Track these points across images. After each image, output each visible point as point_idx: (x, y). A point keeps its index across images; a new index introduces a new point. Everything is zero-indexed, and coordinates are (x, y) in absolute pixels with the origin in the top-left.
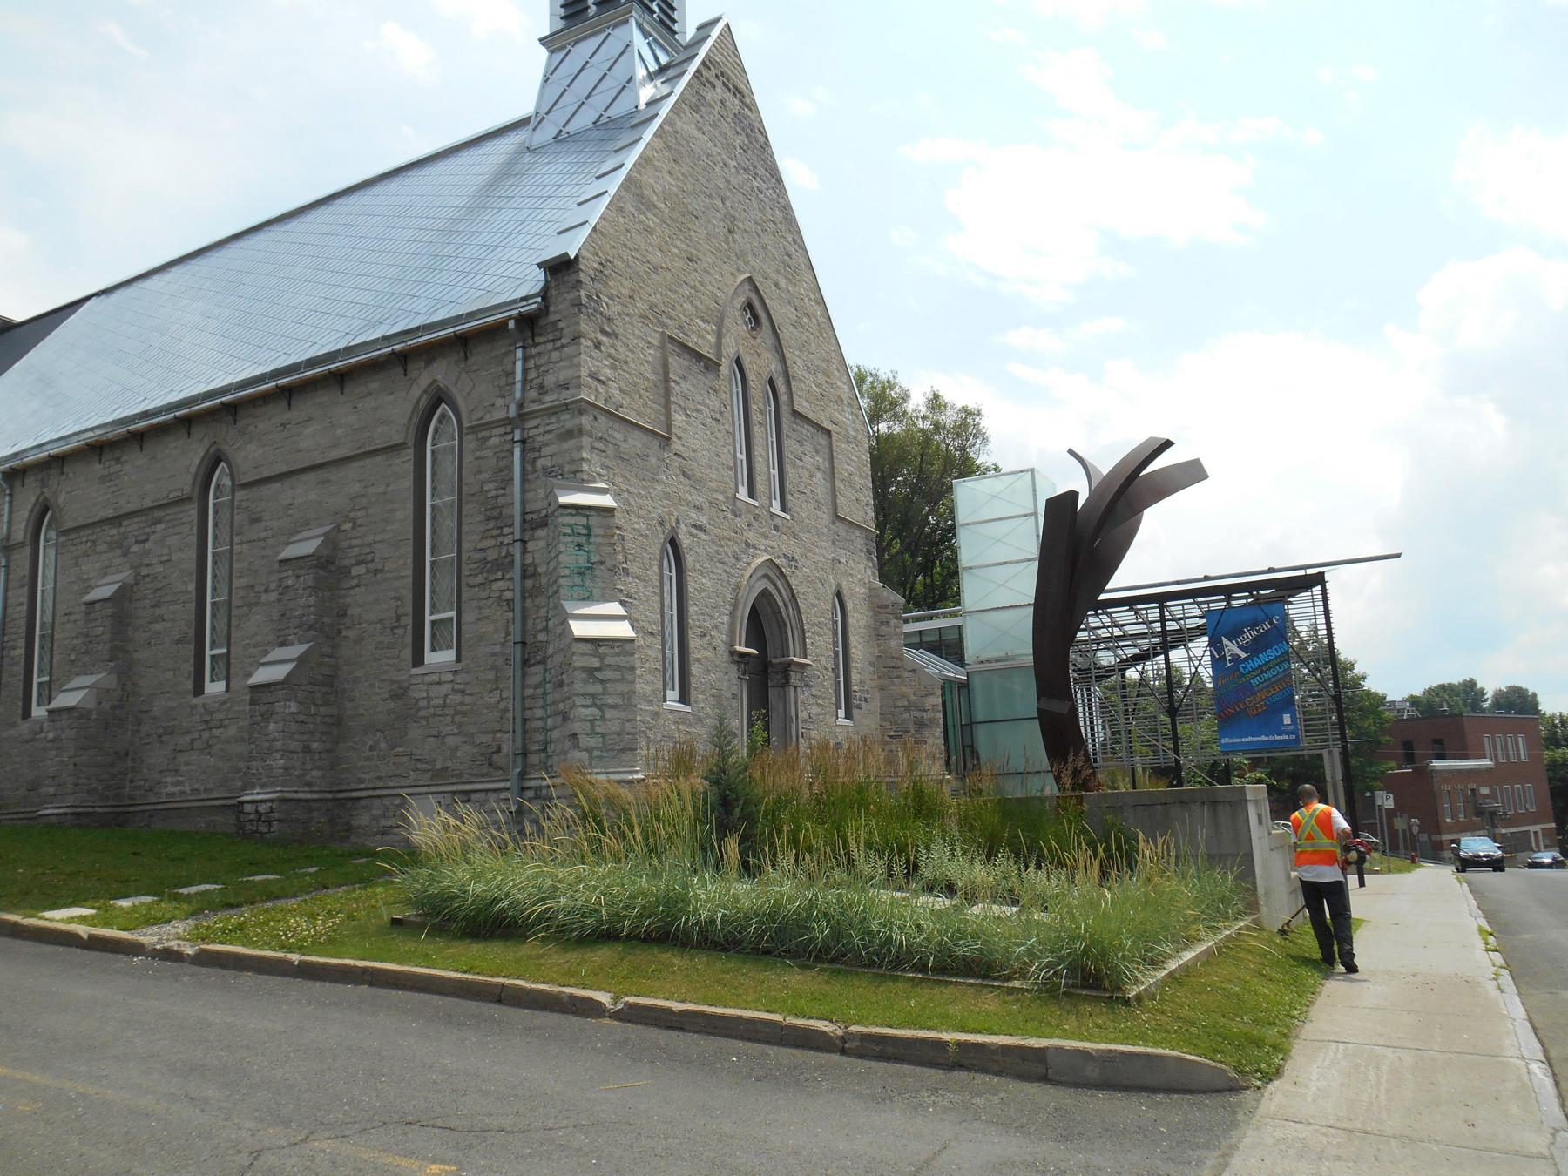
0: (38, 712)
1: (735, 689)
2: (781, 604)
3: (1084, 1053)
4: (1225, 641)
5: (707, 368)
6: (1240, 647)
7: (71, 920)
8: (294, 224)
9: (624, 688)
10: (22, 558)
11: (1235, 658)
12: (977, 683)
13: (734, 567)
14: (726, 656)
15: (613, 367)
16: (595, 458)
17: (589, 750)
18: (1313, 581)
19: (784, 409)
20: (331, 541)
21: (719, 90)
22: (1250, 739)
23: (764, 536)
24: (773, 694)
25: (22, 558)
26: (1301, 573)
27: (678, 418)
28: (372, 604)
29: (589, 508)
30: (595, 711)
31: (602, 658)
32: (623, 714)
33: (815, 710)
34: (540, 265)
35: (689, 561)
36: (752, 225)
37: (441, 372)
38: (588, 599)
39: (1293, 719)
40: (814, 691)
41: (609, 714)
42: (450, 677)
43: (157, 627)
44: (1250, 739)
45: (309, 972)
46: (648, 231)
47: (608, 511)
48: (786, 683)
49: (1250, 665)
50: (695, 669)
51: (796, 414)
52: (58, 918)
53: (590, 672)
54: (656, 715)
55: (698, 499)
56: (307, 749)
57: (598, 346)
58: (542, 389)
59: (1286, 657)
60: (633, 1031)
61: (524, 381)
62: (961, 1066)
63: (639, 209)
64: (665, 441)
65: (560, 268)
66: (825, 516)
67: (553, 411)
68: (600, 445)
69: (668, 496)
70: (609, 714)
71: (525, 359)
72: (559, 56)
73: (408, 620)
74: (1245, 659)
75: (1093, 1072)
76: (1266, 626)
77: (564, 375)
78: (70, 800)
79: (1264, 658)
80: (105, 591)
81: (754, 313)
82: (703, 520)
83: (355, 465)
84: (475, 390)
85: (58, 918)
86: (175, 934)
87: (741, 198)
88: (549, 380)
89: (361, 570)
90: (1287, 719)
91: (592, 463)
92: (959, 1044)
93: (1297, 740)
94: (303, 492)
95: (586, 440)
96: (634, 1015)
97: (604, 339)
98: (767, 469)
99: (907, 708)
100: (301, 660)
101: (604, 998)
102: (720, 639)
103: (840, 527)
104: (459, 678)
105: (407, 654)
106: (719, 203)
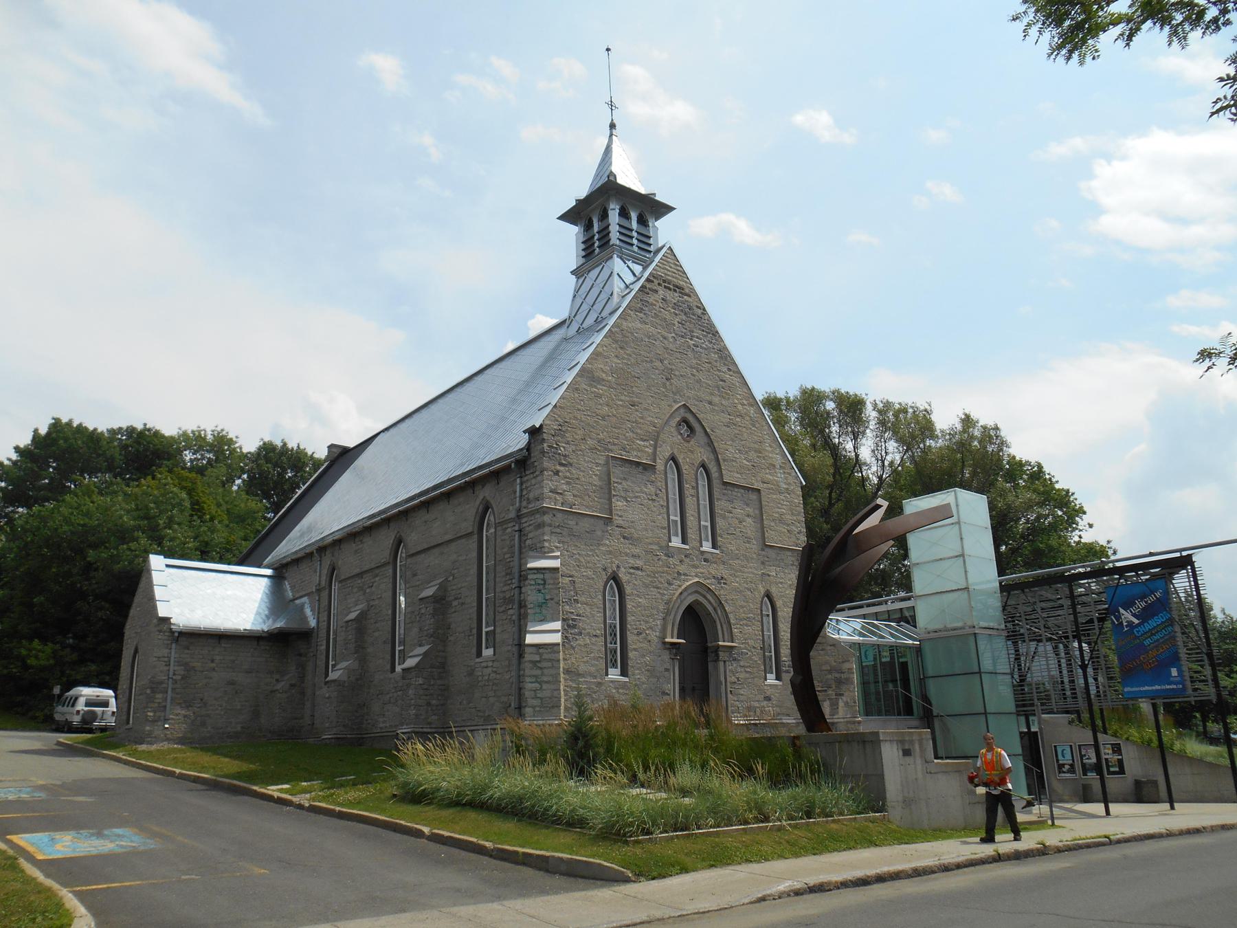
0: (398, 668)
1: (668, 666)
2: (710, 609)
3: (561, 859)
4: (1122, 611)
5: (645, 469)
6: (1134, 615)
7: (281, 791)
8: (433, 407)
9: (552, 672)
10: (325, 594)
11: (1130, 624)
12: (927, 648)
13: (667, 589)
14: (660, 645)
15: (568, 483)
16: (554, 538)
17: (534, 707)
18: (1184, 562)
19: (716, 483)
20: (443, 587)
21: (661, 292)
22: (1147, 688)
23: (695, 567)
24: (710, 665)
25: (325, 594)
26: (1178, 555)
27: (619, 504)
28: (461, 620)
29: (544, 569)
30: (537, 685)
31: (541, 655)
32: (553, 687)
33: (742, 676)
34: (525, 432)
35: (628, 589)
36: (688, 370)
37: (486, 492)
38: (544, 620)
39: (1180, 671)
41: (545, 686)
42: (490, 664)
43: (376, 634)
44: (1147, 688)
45: (341, 816)
46: (599, 396)
47: (555, 570)
48: (717, 660)
49: (1142, 629)
50: (631, 655)
51: (725, 484)
52: (273, 790)
53: (534, 663)
54: (599, 684)
55: (637, 551)
56: (429, 704)
57: (557, 473)
58: (529, 501)
59: (1171, 622)
60: (433, 846)
61: (521, 496)
62: (524, 864)
63: (591, 385)
64: (609, 521)
65: (534, 432)
66: (755, 546)
67: (532, 513)
68: (558, 530)
69: (610, 552)
70: (545, 686)
71: (521, 484)
72: (581, 280)
73: (475, 631)
74: (1139, 625)
75: (563, 868)
76: (1152, 599)
77: (537, 493)
78: (334, 731)
79: (1153, 623)
80: (353, 616)
81: (689, 425)
82: (639, 563)
83: (454, 544)
84: (503, 501)
85: (273, 790)
86: (304, 799)
87: (679, 355)
88: (531, 496)
89: (455, 603)
90: (1174, 672)
91: (550, 541)
92: (524, 854)
93: (1184, 689)
94: (432, 559)
95: (547, 529)
96: (435, 838)
97: (562, 468)
98: (699, 519)
99: (830, 672)
100: (425, 654)
101: (426, 830)
102: (654, 636)
103: (771, 553)
104: (496, 664)
105: (474, 650)
106: (658, 364)
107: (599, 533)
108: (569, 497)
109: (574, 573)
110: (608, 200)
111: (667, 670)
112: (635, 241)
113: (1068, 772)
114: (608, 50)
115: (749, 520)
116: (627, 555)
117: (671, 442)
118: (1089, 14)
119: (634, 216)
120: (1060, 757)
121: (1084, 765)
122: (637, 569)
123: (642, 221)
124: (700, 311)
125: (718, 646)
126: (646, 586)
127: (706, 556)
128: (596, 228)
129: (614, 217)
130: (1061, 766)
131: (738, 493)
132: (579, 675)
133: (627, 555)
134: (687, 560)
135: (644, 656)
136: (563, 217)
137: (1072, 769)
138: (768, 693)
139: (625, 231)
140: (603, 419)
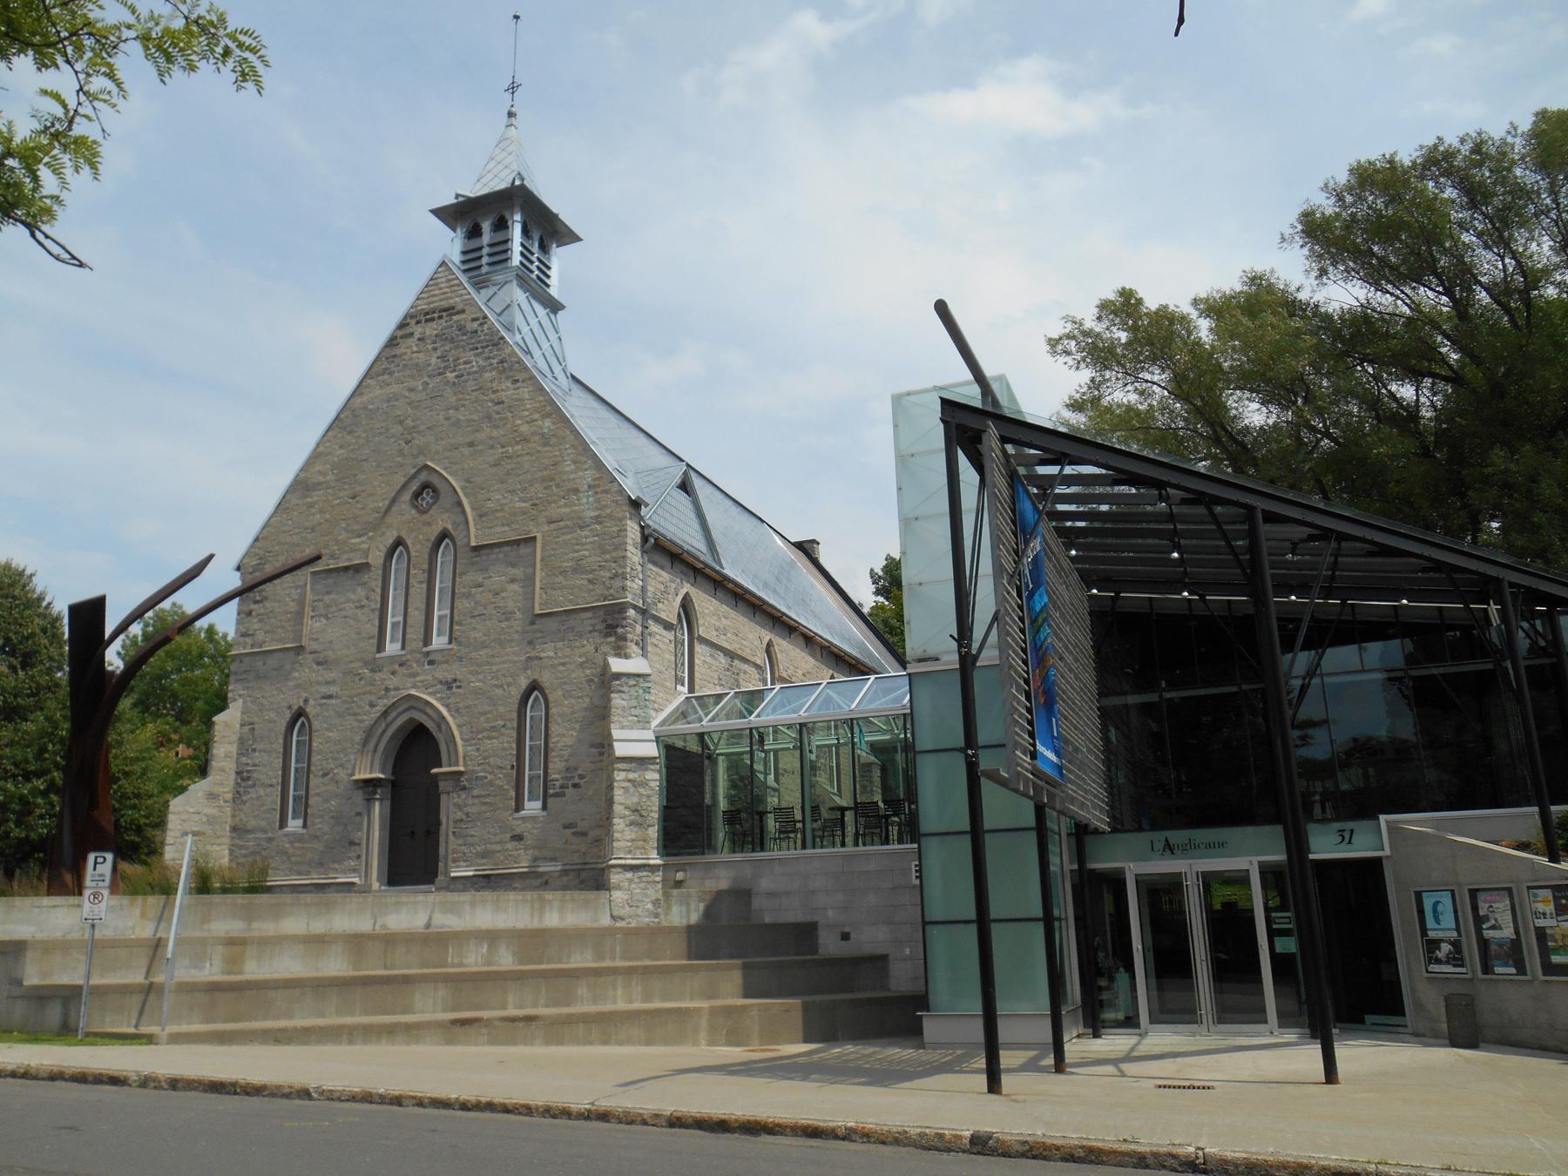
8: (718, 493)
40: (476, 792)
54: (270, 840)
69: (298, 686)
81: (426, 490)
82: (333, 690)
87: (429, 403)
107: (288, 667)
108: (260, 636)
109: (255, 719)
111: (359, 814)
113: (1449, 960)
114: (517, 17)
115: (515, 587)
116: (318, 683)
117: (404, 518)
119: (486, 226)
120: (1430, 923)
121: (1484, 944)
122: (330, 697)
124: (475, 325)
125: (437, 775)
127: (431, 657)
128: (486, 238)
130: (1433, 945)
131: (498, 554)
132: (248, 832)
133: (318, 683)
134: (403, 670)
135: (327, 801)
136: (578, 239)
137: (1456, 958)
138: (518, 831)
140: (313, 530)
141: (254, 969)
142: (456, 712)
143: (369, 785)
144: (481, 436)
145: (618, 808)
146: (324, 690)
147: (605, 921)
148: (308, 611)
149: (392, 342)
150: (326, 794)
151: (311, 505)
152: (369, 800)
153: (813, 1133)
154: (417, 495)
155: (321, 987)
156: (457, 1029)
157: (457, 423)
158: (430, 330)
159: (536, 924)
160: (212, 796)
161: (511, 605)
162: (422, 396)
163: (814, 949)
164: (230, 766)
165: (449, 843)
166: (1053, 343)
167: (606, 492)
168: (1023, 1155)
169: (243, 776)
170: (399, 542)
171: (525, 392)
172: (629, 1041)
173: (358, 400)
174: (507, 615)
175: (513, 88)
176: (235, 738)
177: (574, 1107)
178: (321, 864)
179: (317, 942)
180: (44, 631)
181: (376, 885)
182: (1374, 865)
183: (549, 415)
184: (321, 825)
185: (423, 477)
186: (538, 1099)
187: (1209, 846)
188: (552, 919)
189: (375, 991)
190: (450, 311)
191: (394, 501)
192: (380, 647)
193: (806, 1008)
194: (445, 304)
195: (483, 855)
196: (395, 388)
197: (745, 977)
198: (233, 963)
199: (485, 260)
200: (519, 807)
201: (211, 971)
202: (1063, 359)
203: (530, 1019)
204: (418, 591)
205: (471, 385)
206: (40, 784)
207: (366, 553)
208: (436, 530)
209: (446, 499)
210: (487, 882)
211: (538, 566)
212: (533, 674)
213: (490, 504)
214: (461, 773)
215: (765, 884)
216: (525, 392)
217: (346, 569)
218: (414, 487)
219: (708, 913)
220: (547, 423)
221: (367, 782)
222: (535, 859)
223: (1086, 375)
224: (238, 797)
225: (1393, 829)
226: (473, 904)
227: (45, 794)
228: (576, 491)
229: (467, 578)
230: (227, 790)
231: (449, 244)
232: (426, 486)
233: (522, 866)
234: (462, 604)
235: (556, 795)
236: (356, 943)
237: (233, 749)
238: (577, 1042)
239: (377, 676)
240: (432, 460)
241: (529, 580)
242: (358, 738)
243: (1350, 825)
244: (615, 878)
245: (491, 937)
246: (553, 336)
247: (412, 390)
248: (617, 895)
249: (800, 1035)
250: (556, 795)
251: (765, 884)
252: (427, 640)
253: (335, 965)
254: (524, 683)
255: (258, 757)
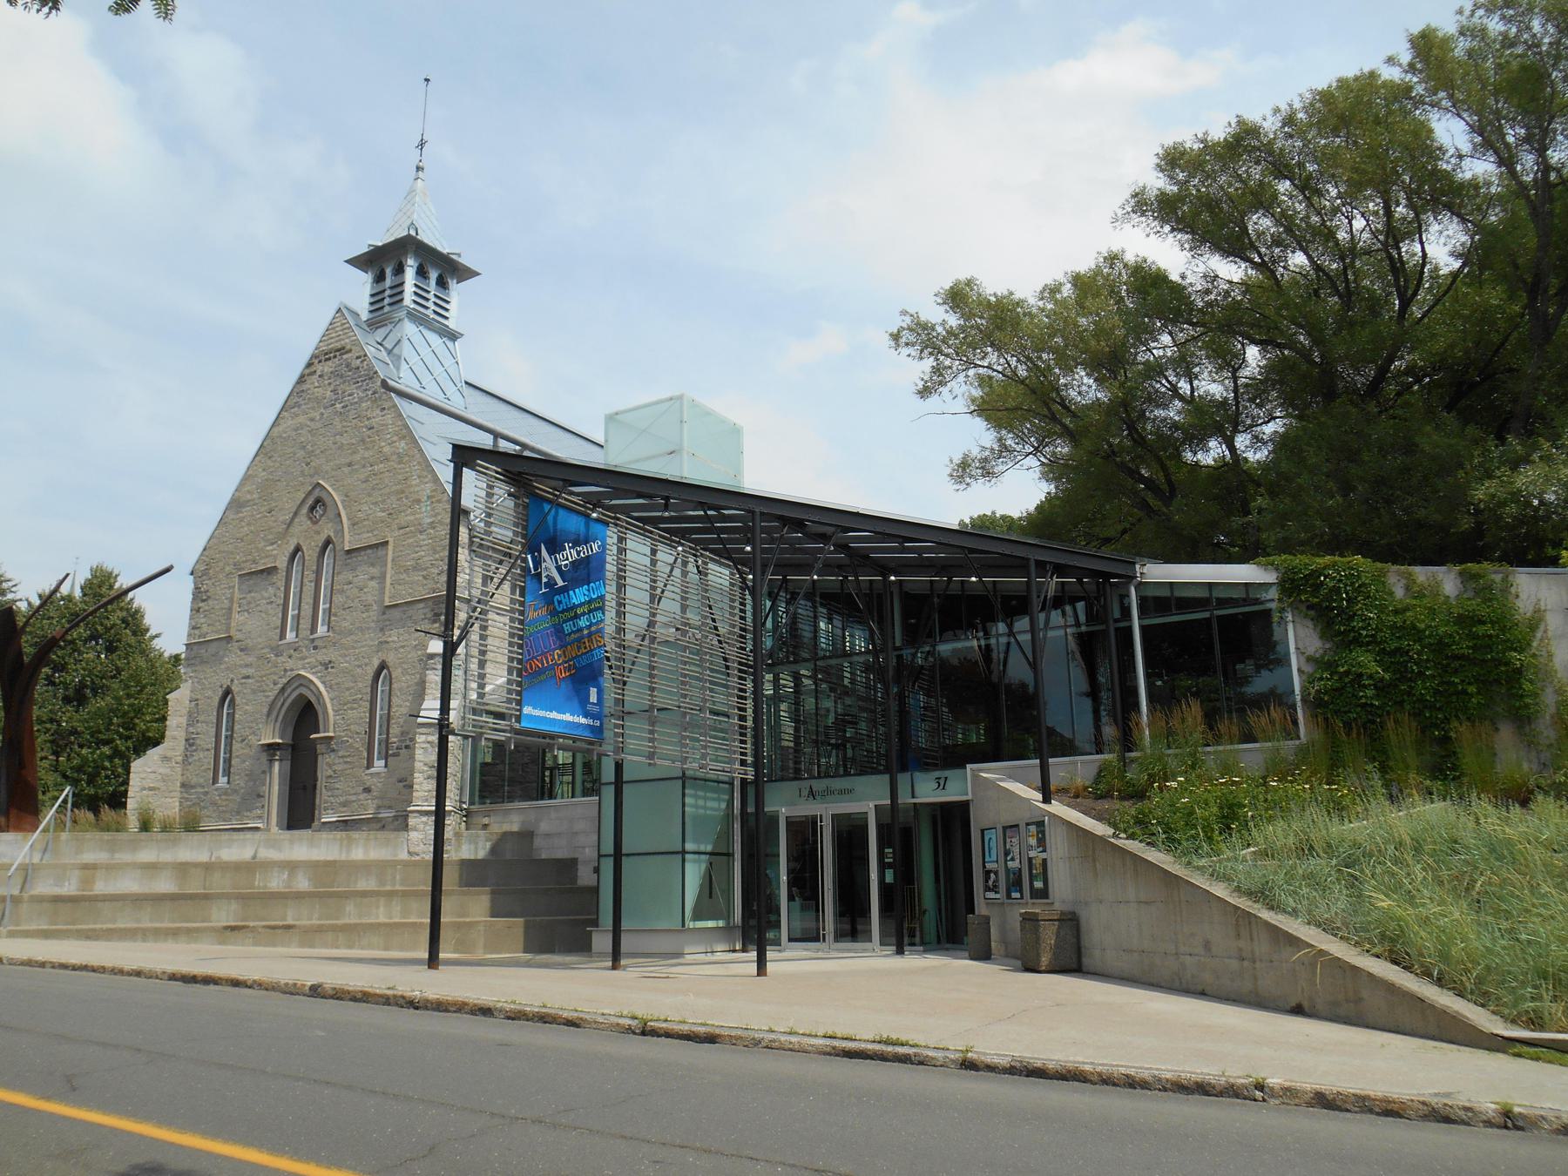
44: (554, 715)
54: (206, 793)
55: (250, 660)
81: (317, 504)
82: (250, 671)
110: (405, 254)
112: (430, 304)
115: (373, 583)
118: (890, 866)
119: (388, 272)
123: (442, 283)
126: (254, 692)
128: (388, 282)
129: (410, 275)
131: (363, 556)
134: (296, 654)
139: (421, 293)
141: (101, 887)
142: (329, 687)
143: (271, 748)
144: (357, 457)
145: (418, 765)
146: (245, 671)
147: (404, 856)
148: (235, 605)
149: (301, 380)
150: (245, 756)
151: (242, 520)
152: (271, 761)
153: (236, 983)
154: (312, 508)
155: (138, 900)
156: (228, 933)
157: (341, 447)
158: (327, 368)
159: (343, 857)
160: (165, 759)
161: (370, 598)
162: (318, 425)
163: (574, 878)
164: (181, 735)
165: (323, 796)
166: (896, 337)
167: (439, 501)
168: (332, 997)
169: (190, 742)
170: (298, 549)
171: (389, 418)
172: (370, 946)
173: (275, 430)
174: (367, 607)
175: (422, 144)
176: (185, 711)
177: (127, 968)
178: (238, 813)
179: (152, 868)
180: (124, 621)
181: (274, 829)
182: (965, 806)
183: (404, 437)
184: (239, 781)
185: (317, 493)
186: (109, 964)
187: (841, 792)
188: (358, 854)
189: (257, 909)
190: (342, 350)
191: (296, 514)
192: (282, 636)
193: (527, 927)
194: (338, 345)
195: (344, 804)
196: (301, 419)
197: (493, 901)
198: (87, 882)
199: (387, 301)
200: (370, 765)
201: (69, 888)
202: (905, 351)
203: (289, 927)
204: (309, 587)
205: (352, 414)
206: (106, 750)
207: (275, 557)
208: (323, 537)
209: (331, 513)
210: (345, 825)
211: (389, 565)
212: (382, 656)
213: (360, 515)
214: (331, 738)
215: (544, 827)
216: (389, 418)
217: (262, 571)
218: (310, 501)
219: (493, 851)
220: (403, 444)
221: (269, 745)
222: (379, 807)
223: (929, 363)
224: (186, 761)
225: (975, 777)
226: (292, 842)
227: (110, 758)
228: (418, 501)
229: (341, 577)
230: (178, 754)
231: (358, 290)
232: (318, 501)
233: (368, 814)
234: (338, 599)
235: (394, 755)
236: (182, 869)
237: (184, 721)
238: (325, 946)
239: (280, 659)
240: (327, 480)
241: (383, 577)
242: (265, 710)
243: (947, 773)
244: (412, 821)
245: (292, 866)
246: (448, 362)
247: (312, 420)
248: (413, 835)
249: (521, 946)
250: (394, 755)
251: (544, 827)
252: (313, 629)
253: (165, 885)
254: (376, 663)
255: (200, 727)
